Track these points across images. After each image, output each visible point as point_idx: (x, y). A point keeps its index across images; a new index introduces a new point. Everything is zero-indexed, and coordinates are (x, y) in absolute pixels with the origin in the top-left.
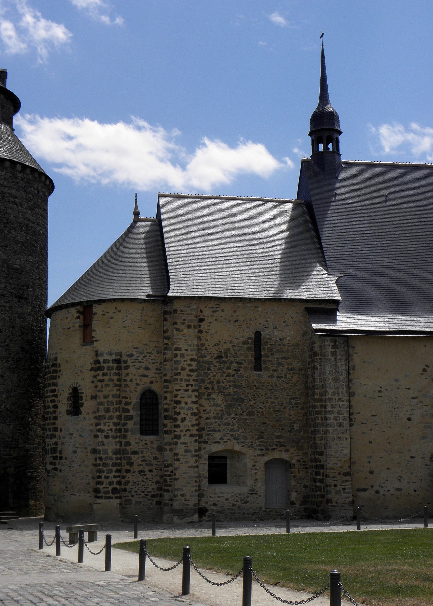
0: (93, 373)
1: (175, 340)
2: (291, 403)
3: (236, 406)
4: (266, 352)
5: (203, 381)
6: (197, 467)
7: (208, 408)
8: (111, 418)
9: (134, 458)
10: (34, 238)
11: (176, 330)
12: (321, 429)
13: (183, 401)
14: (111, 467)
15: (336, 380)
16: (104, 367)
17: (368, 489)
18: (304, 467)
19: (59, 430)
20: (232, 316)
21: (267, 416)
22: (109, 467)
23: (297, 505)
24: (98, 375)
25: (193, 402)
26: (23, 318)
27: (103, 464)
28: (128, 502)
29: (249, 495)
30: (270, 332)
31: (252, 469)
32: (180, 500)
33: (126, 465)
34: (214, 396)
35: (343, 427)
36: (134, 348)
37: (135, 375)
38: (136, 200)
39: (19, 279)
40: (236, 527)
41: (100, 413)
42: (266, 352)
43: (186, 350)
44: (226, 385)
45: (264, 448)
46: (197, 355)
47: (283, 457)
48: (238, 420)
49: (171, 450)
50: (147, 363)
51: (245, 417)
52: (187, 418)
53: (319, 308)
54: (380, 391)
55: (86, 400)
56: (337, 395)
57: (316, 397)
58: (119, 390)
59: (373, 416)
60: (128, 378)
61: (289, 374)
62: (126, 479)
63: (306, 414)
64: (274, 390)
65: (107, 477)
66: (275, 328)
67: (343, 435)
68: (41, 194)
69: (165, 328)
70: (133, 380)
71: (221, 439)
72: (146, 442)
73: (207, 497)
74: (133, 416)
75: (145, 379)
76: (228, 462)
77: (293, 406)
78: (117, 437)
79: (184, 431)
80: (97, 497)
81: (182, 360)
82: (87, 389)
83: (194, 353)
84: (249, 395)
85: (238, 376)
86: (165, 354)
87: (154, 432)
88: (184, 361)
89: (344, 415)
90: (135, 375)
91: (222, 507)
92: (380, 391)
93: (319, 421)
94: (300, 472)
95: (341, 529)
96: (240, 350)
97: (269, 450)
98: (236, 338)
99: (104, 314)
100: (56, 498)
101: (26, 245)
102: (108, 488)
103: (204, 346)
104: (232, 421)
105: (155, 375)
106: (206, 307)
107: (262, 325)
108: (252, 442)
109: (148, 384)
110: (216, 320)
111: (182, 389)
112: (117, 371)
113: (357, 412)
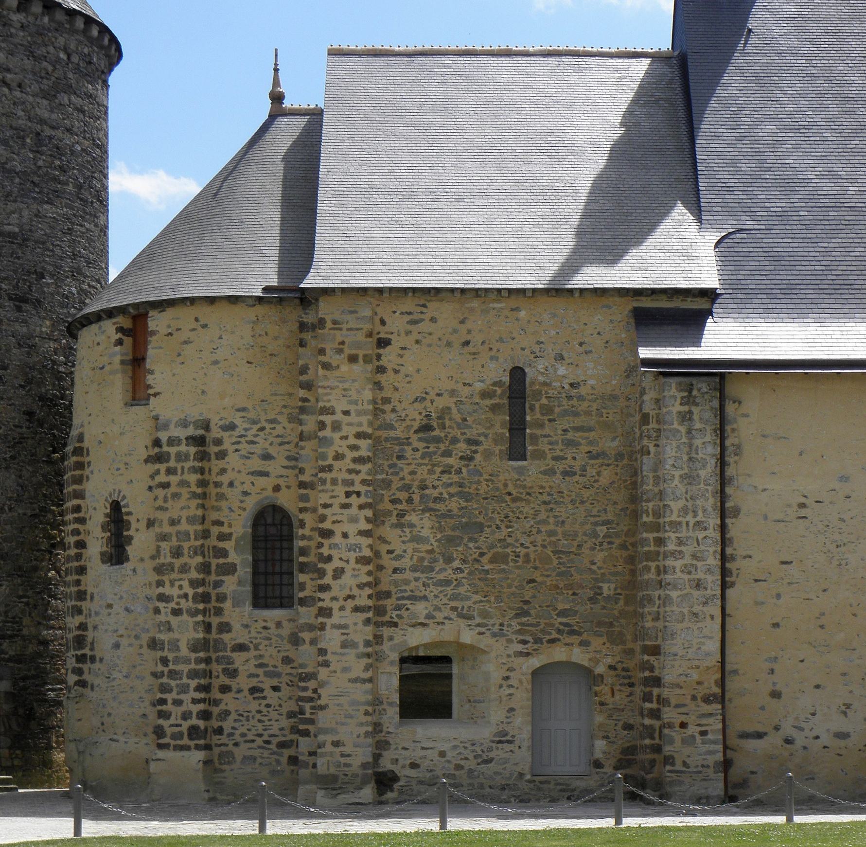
0: (152, 467)
1: (320, 391)
2: (595, 535)
3: (465, 541)
4: (538, 416)
5: (387, 484)
6: (370, 680)
7: (397, 546)
8: (184, 569)
9: (238, 659)
10: (58, 163)
11: (323, 368)
12: (657, 593)
13: (338, 529)
14: (185, 680)
15: (689, 479)
16: (168, 454)
17: (766, 734)
18: (626, 681)
19: (88, 597)
20: (455, 331)
21: (537, 564)
22: (181, 679)
23: (608, 769)
24: (158, 472)
25: (361, 533)
26: (30, 347)
27: (170, 671)
28: (227, 757)
29: (494, 745)
30: (546, 369)
31: (501, 686)
32: (331, 754)
33: (221, 676)
34: (413, 518)
35: (706, 589)
36: (238, 410)
37: (239, 472)
38: (276, 65)
39: (18, 258)
40: (567, 817)
41: (162, 557)
42: (538, 416)
43: (346, 413)
44: (441, 494)
45: (529, 638)
46: (370, 424)
47: (574, 659)
48: (470, 573)
49: (313, 642)
50: (267, 445)
51: (486, 567)
52: (348, 568)
53: (668, 310)
54: (802, 506)
55: (137, 530)
56: (691, 514)
57: (645, 519)
58: (203, 506)
59: (783, 563)
60: (225, 479)
61: (593, 465)
62: (222, 707)
63: (631, 560)
64: (556, 503)
65: (178, 703)
66: (560, 358)
67: (705, 609)
68: (75, 59)
69: (301, 362)
70: (236, 483)
71: (429, 616)
72: (265, 624)
73: (397, 749)
74: (235, 565)
75: (262, 481)
76: (455, 670)
77: (600, 540)
78: (197, 612)
79: (341, 599)
80: (161, 746)
81: (336, 436)
82: (138, 508)
83: (364, 419)
84: (496, 515)
85: (468, 471)
86: (301, 422)
87: (285, 601)
88: (341, 438)
89: (708, 562)
90: (239, 472)
91: (431, 771)
92: (802, 506)
93: (652, 575)
94: (616, 693)
95: (282, 828)
96: (475, 411)
97: (542, 643)
98: (465, 384)
99: (171, 334)
100: (81, 748)
101: (36, 179)
102: (180, 725)
103: (390, 402)
104: (454, 576)
105: (284, 472)
106: (395, 312)
107: (527, 352)
108: (501, 625)
109: (269, 492)
110: (417, 342)
111: (336, 502)
112: (198, 464)
113: (744, 553)
